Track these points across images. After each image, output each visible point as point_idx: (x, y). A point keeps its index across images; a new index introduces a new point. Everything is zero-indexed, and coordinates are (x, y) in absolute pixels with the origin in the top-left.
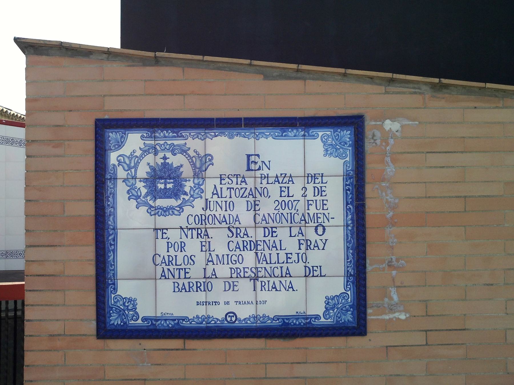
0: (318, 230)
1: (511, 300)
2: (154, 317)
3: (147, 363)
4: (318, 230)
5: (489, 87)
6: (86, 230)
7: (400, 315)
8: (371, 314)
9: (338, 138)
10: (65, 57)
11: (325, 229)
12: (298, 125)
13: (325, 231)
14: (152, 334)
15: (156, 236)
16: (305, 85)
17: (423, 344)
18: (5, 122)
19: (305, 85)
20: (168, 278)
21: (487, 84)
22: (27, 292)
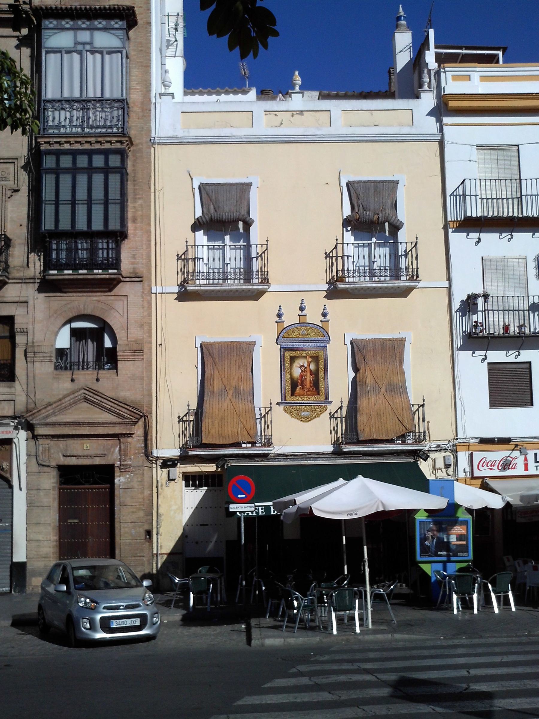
2: (87, 360)
18: (439, 553)
20: (524, 313)
22: (484, 368)
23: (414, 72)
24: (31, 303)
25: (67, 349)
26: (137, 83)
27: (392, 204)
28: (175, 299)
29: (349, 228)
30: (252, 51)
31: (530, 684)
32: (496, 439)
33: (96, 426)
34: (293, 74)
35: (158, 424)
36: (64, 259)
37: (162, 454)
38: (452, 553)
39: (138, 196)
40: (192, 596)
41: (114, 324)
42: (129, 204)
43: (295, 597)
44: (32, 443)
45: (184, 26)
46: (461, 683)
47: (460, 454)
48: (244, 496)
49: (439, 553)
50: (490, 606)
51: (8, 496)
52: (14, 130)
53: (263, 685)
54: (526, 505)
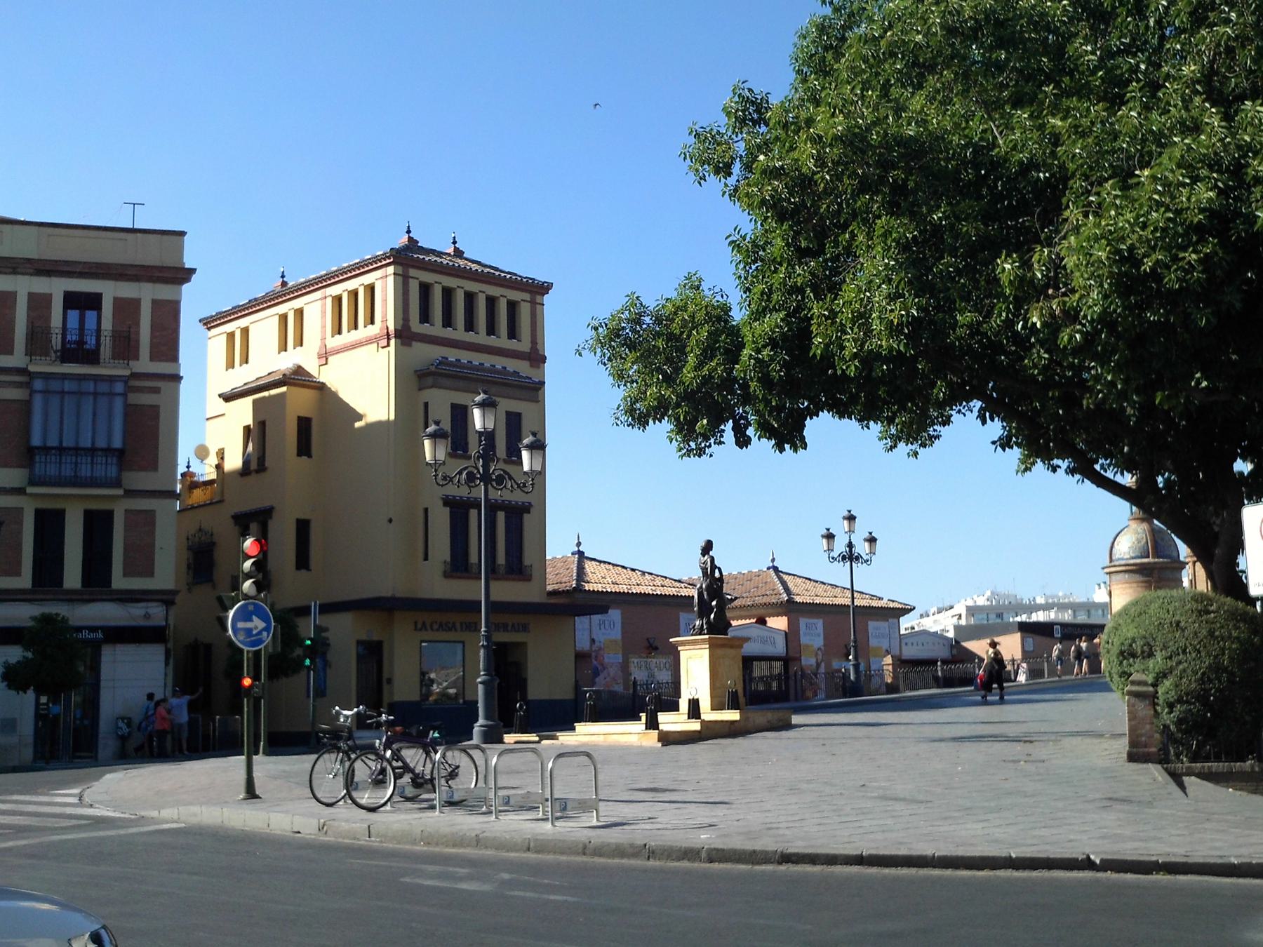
11: (418, 242)
24: (369, 823)
28: (220, 396)
30: (810, 355)
31: (1261, 856)
46: (1083, 405)
48: (671, 640)
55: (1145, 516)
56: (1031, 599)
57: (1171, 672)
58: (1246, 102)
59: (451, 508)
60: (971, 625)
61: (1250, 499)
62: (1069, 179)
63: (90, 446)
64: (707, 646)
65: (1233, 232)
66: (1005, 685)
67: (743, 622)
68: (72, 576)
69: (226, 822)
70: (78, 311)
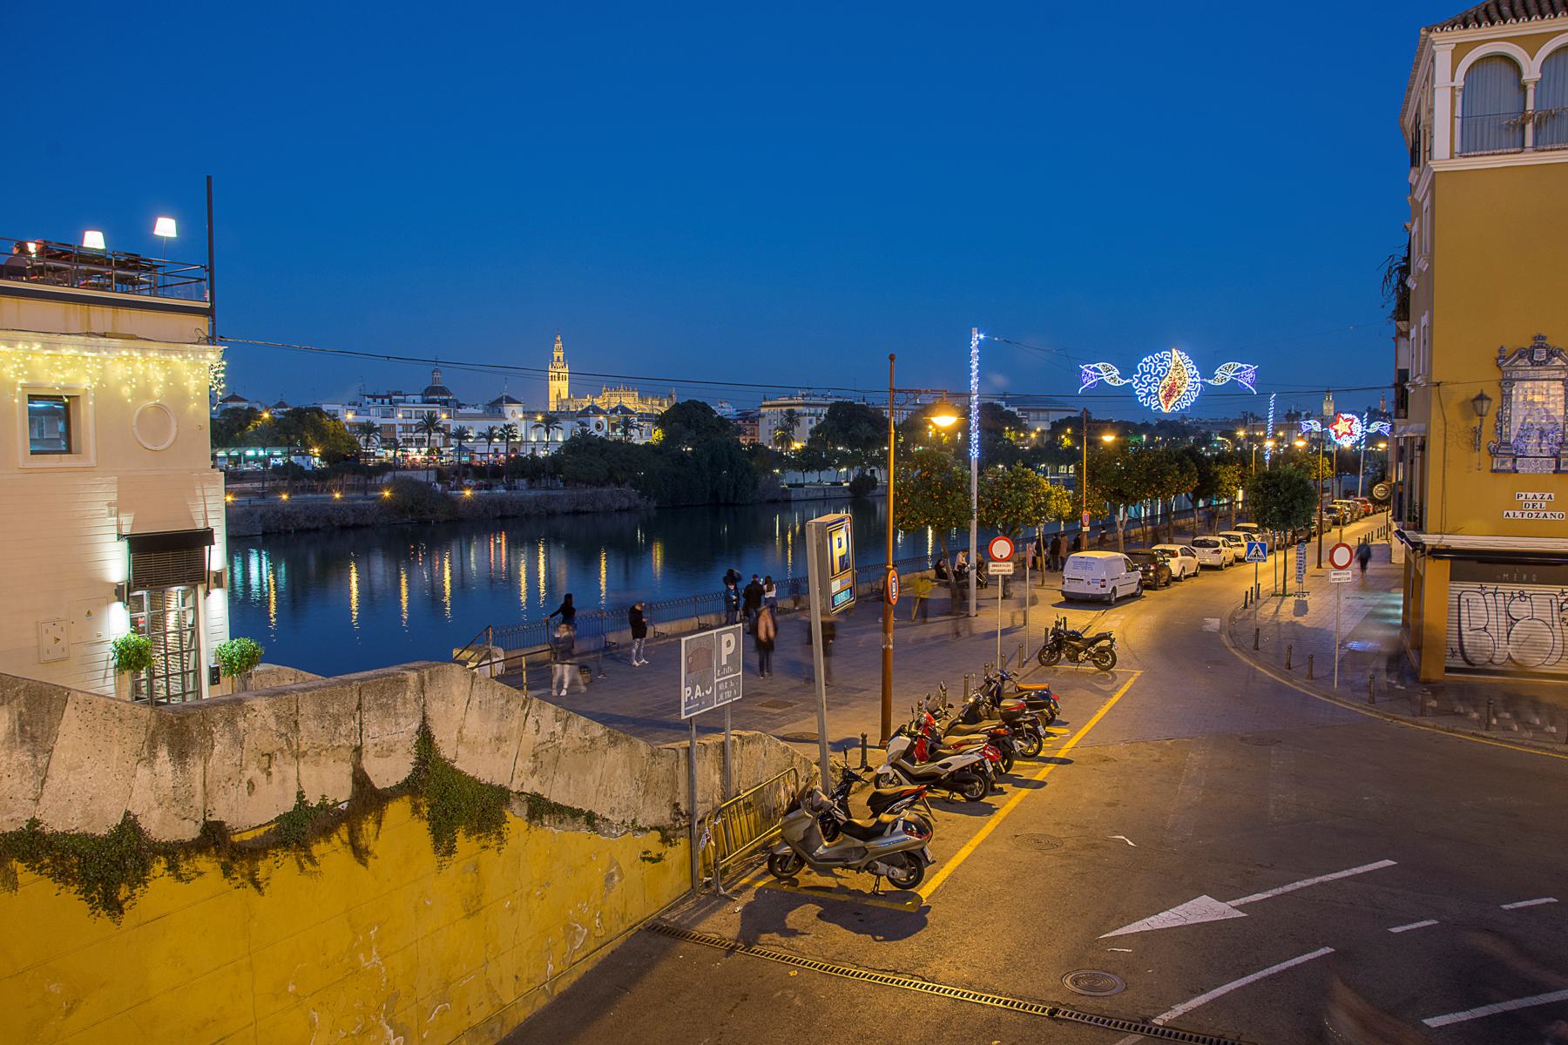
0: (1057, 421)
1: (424, 713)
3: (915, 577)
4: (1057, 421)
5: (1532, 104)
6: (278, 867)
7: (794, 689)
8: (1560, 395)
9: (982, 794)
10: (321, 806)
12: (221, 453)
13: (1060, 420)
14: (1535, 396)
15: (1478, 141)
16: (462, 575)
17: (1068, 625)
18: (780, 830)
19: (462, 575)
21: (425, 480)
23: (483, 547)
25: (214, 588)
26: (676, 805)
27: (767, 665)
29: (310, 805)
32: (886, 448)
33: (735, 881)
34: (1330, 947)
35: (1377, 386)
36: (96, 383)
37: (420, 389)
38: (846, 487)
39: (1021, 768)
40: (930, 532)
41: (103, 311)
42: (569, 422)
43: (1367, 445)
44: (1065, 708)
45: (561, 993)
47: (567, 397)
49: (780, 830)
50: (987, 401)
51: (1554, 389)
52: (993, 807)
53: (1332, 953)
54: (628, 625)
55: (455, 548)
56: (308, 866)
57: (304, 757)
58: (657, 435)
59: (786, 928)
60: (1404, 596)
61: (567, 547)
62: (872, 936)
63: (868, 744)
64: (1402, 595)
65: (561, 645)
66: (1016, 762)
67: (542, 575)
68: (1478, 147)
69: (400, 801)
70: (85, 245)
